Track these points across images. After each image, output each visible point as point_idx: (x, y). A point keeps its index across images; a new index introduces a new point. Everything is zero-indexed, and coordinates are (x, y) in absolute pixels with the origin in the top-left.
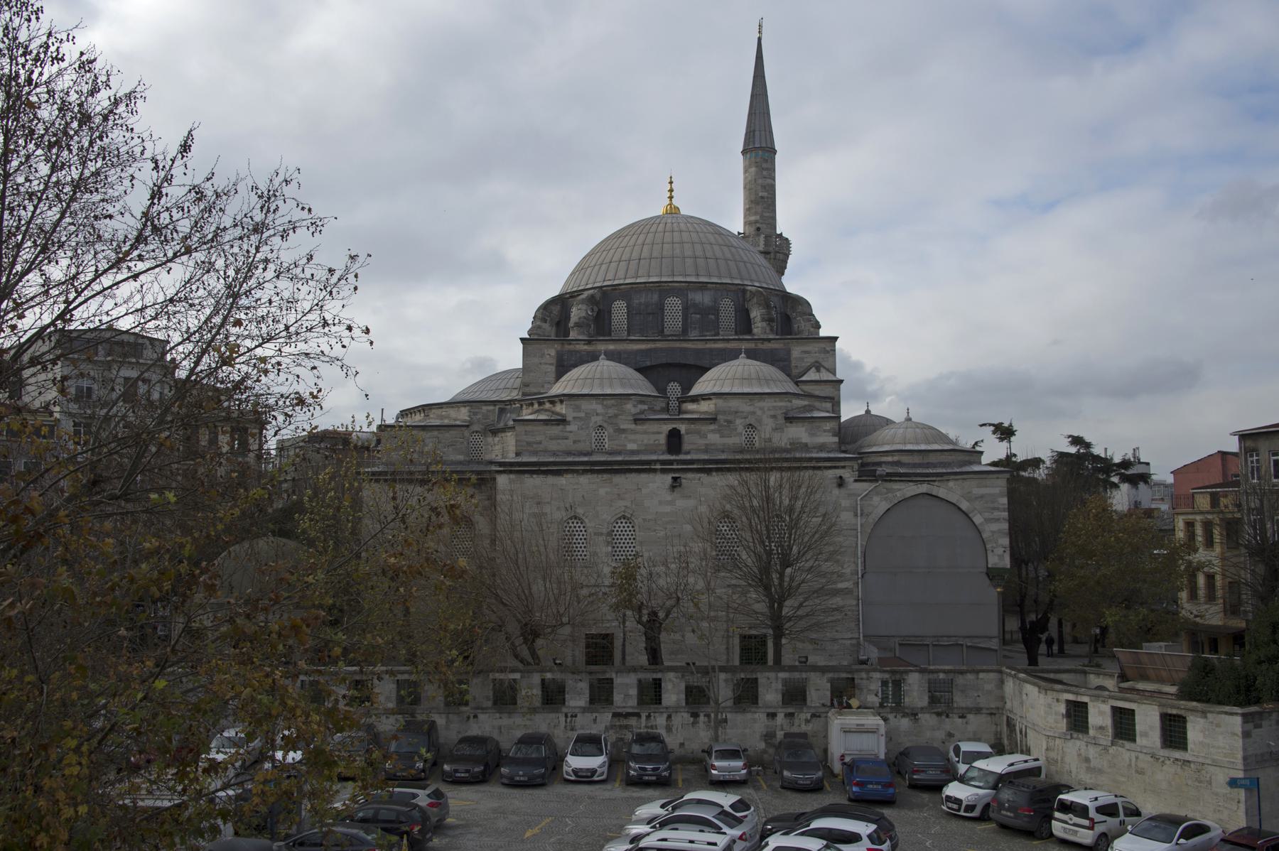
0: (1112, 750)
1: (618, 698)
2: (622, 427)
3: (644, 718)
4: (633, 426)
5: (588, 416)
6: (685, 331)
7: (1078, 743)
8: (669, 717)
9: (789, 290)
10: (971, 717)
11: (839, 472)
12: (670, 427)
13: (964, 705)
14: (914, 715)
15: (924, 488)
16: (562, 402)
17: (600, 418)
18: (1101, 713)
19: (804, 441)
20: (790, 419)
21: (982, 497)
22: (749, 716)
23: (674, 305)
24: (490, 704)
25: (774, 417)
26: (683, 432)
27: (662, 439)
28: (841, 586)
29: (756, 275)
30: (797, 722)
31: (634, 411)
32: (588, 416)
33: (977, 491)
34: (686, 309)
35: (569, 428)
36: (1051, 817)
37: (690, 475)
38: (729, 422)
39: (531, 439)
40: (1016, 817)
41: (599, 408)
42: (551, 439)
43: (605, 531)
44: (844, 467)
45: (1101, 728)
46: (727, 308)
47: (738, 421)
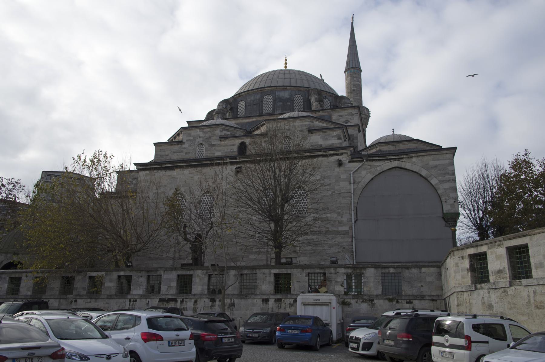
0: (511, 291)
1: (163, 288)
4: (219, 143)
5: (195, 139)
6: (274, 110)
7: (481, 292)
8: (196, 302)
9: (340, 95)
11: (340, 157)
12: (240, 141)
14: (371, 300)
15: (396, 164)
17: (201, 139)
18: (498, 257)
19: (320, 144)
21: (436, 166)
22: (250, 301)
23: (268, 99)
24: (84, 292)
25: (301, 131)
26: (247, 143)
27: (235, 149)
28: (341, 229)
30: (283, 306)
31: (220, 134)
33: (432, 163)
34: (274, 101)
35: (184, 146)
36: (430, 344)
39: (163, 154)
40: (396, 345)
41: (201, 134)
44: (342, 154)
45: (500, 272)
46: (299, 99)
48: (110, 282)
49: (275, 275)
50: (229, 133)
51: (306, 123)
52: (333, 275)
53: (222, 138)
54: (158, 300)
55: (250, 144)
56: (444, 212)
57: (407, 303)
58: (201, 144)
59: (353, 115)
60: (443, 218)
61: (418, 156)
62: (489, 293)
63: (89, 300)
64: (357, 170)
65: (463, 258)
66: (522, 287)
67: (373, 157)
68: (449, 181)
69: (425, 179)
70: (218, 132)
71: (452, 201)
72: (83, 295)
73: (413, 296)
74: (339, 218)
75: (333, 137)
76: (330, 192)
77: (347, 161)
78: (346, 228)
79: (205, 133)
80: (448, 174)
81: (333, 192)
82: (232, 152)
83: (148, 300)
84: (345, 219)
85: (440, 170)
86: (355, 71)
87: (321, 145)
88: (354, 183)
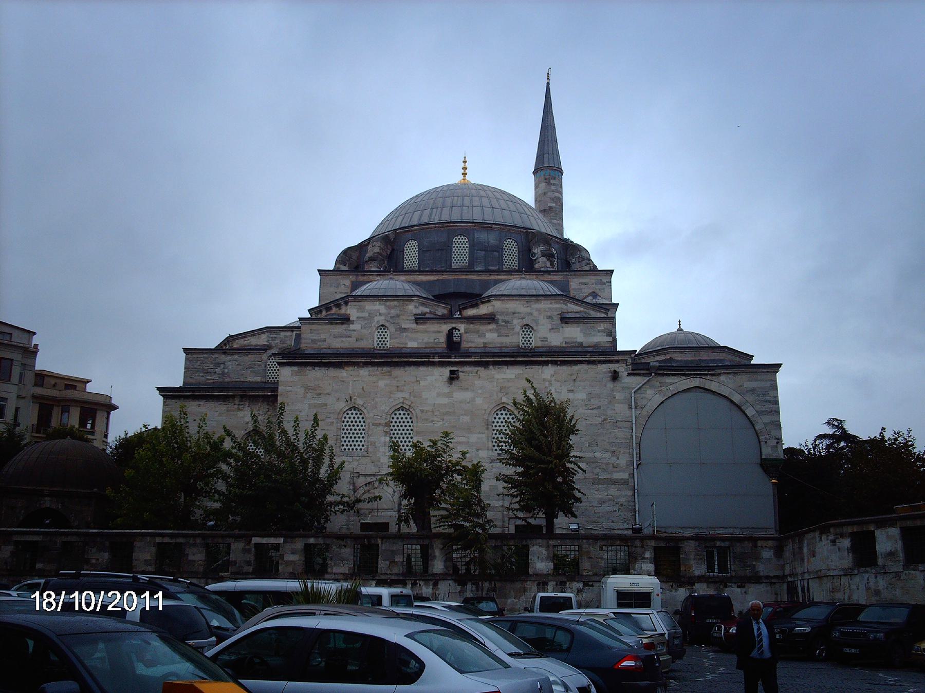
2: (403, 326)
4: (414, 326)
5: (371, 316)
6: (472, 262)
7: (866, 576)
11: (613, 367)
16: (346, 303)
17: (383, 318)
19: (579, 340)
20: (565, 320)
25: (550, 317)
27: (442, 339)
29: (541, 225)
32: (371, 316)
34: (473, 246)
35: (352, 327)
37: (467, 369)
38: (507, 322)
43: (383, 422)
44: (617, 362)
47: (515, 322)
48: (292, 553)
51: (558, 307)
53: (420, 319)
55: (466, 333)
58: (383, 325)
60: (761, 465)
61: (728, 374)
62: (876, 577)
64: (640, 388)
66: (917, 572)
69: (738, 407)
70: (413, 308)
71: (774, 442)
72: (247, 573)
78: (625, 476)
79: (389, 308)
80: (770, 401)
81: (605, 420)
84: (623, 461)
86: (552, 173)
88: (636, 407)
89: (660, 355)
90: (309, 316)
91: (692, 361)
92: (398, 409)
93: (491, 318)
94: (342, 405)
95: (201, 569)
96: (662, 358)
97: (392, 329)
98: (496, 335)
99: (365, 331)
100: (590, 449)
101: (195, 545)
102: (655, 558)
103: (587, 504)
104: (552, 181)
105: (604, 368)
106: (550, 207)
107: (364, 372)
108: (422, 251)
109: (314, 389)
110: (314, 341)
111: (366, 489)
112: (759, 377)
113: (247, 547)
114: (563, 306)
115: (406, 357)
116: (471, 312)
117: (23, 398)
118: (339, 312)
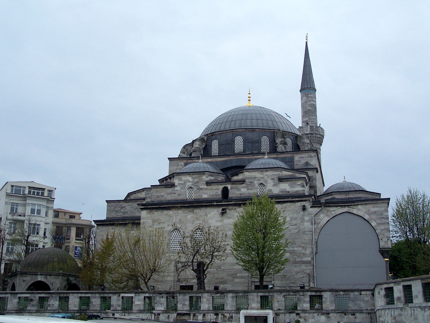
1: (179, 306)
3: (192, 316)
4: (206, 187)
5: (185, 183)
6: (244, 151)
8: (204, 315)
10: (357, 315)
11: (303, 203)
12: (223, 186)
13: (354, 308)
16: (173, 177)
17: (190, 183)
19: (288, 190)
20: (281, 180)
21: (375, 212)
24: (120, 308)
25: (273, 179)
26: (229, 188)
27: (220, 192)
28: (305, 259)
32: (185, 183)
35: (176, 189)
37: (230, 207)
38: (251, 182)
42: (168, 194)
44: (305, 201)
47: (256, 182)
48: (139, 301)
49: (261, 296)
50: (213, 178)
52: (302, 297)
53: (208, 183)
54: (176, 314)
55: (231, 189)
56: (381, 247)
57: (352, 315)
58: (191, 187)
59: (312, 157)
60: (380, 251)
61: (362, 204)
63: (124, 314)
65: (382, 289)
67: (329, 204)
68: (384, 223)
70: (206, 178)
72: (119, 310)
73: (355, 310)
74: (303, 251)
75: (298, 185)
76: (297, 231)
77: (310, 206)
78: (309, 259)
80: (384, 218)
82: (217, 195)
83: (168, 314)
84: (308, 251)
85: (378, 215)
87: (289, 192)
88: (315, 224)
89: (329, 196)
90: (158, 184)
91: (345, 199)
92: (197, 229)
93: (243, 182)
94: (170, 228)
95: (99, 309)
96: (330, 197)
97: (195, 189)
98: (246, 189)
99: (182, 191)
100: (292, 246)
101: (95, 297)
102: (310, 301)
103: (290, 274)
104: (309, 95)
105: (299, 204)
106: (309, 110)
107: (180, 212)
108: (220, 145)
109: (157, 221)
110: (158, 197)
111: (183, 269)
112: (378, 205)
113: (119, 298)
114: (281, 173)
115: (200, 203)
116: (235, 178)
117: (48, 224)
118: (170, 181)
